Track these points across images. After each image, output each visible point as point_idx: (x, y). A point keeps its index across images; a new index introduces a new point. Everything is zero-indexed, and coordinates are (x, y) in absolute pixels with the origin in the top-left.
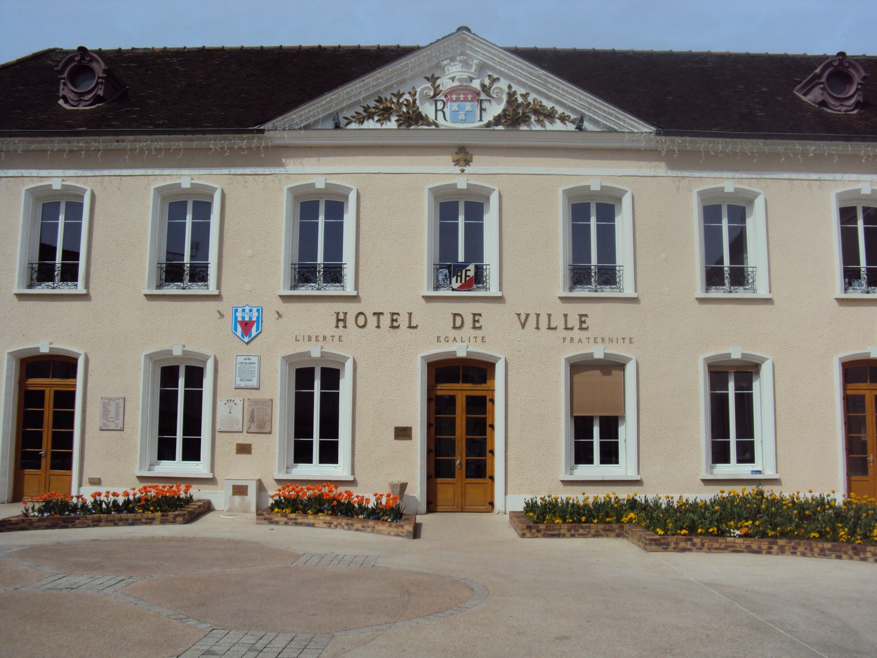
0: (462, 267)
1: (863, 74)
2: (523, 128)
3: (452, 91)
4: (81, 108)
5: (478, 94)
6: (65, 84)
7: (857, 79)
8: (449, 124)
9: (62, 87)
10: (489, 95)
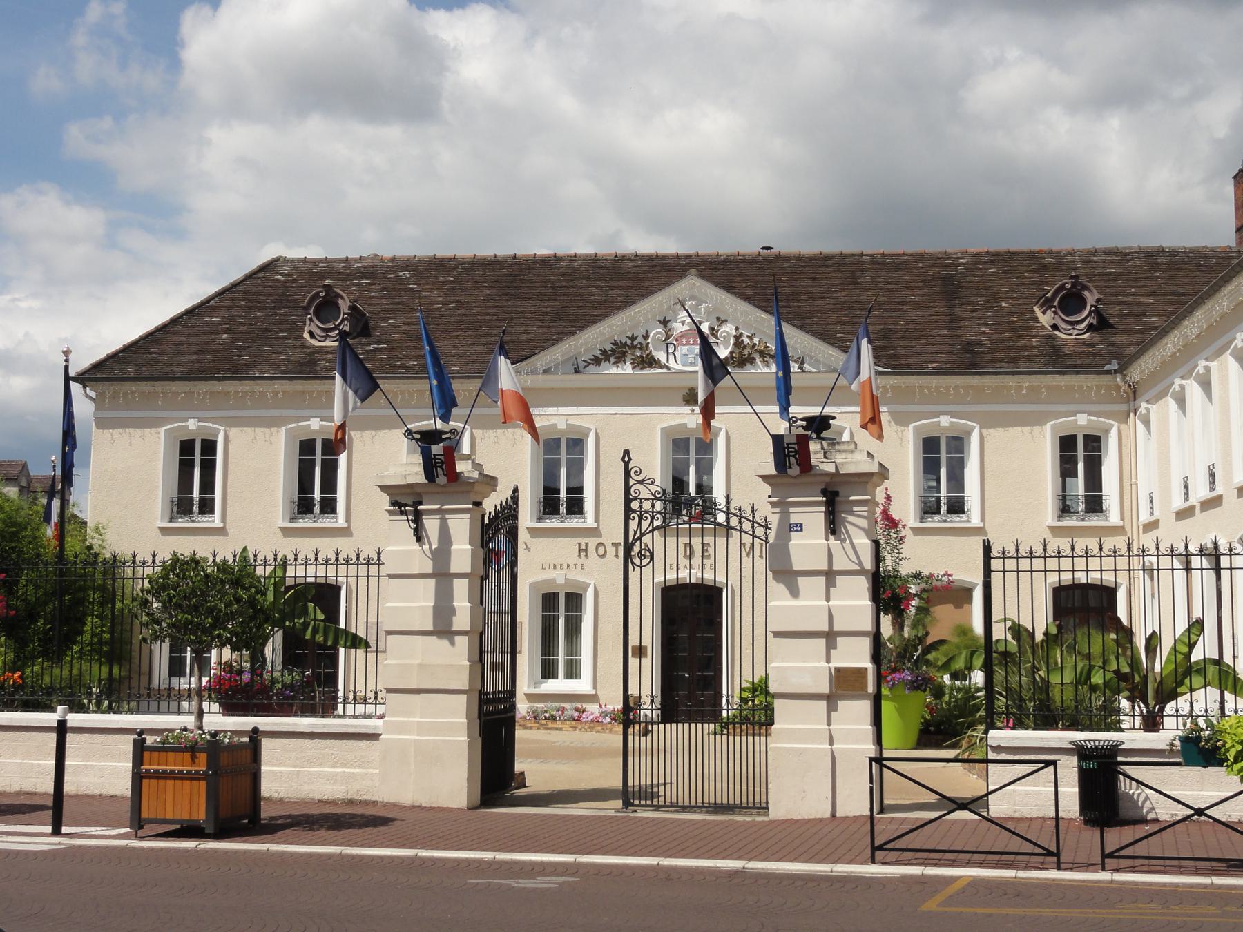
1: (1097, 296)
3: (683, 335)
6: (311, 319)
8: (679, 367)
9: (308, 322)
10: (716, 337)
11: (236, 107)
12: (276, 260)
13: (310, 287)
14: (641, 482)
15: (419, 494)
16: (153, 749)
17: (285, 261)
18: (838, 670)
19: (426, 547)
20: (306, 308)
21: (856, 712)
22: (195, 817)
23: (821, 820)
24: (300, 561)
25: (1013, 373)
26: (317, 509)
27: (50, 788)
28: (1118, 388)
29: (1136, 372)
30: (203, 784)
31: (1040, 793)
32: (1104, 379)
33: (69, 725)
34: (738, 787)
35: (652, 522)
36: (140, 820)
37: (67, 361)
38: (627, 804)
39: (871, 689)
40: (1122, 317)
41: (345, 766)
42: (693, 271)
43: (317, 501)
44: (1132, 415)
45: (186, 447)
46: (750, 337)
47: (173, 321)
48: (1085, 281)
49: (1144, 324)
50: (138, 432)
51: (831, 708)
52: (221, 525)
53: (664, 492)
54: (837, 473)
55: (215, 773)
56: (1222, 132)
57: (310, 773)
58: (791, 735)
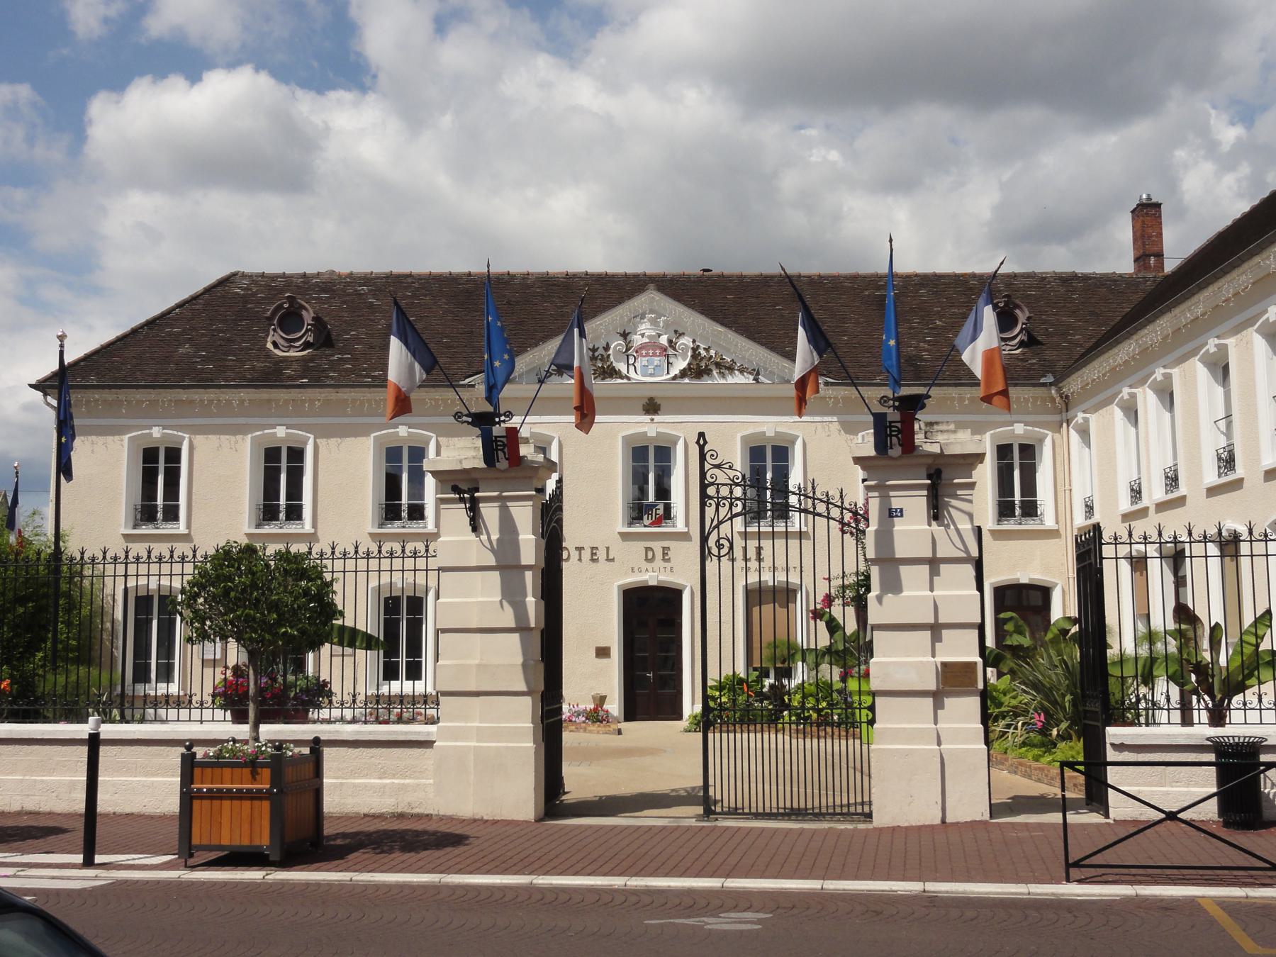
0: (652, 506)
1: (1027, 314)
3: (643, 347)
4: (292, 353)
5: (666, 350)
6: (274, 330)
10: (675, 349)
11: (140, 176)
12: (234, 274)
13: (270, 300)
14: (718, 467)
15: (476, 481)
16: (204, 765)
17: (244, 275)
18: (944, 664)
19: (484, 537)
20: (270, 319)
21: (964, 713)
22: (257, 842)
23: (932, 827)
24: (337, 554)
25: (956, 385)
26: (282, 516)
27: (81, 807)
28: (1053, 400)
29: (1073, 384)
30: (266, 805)
31: (1167, 793)
32: (1040, 392)
33: (102, 737)
35: (730, 508)
36: (190, 847)
37: (62, 346)
38: (708, 813)
40: (1049, 335)
41: (394, 776)
42: (652, 286)
43: (283, 508)
44: (1065, 425)
45: (150, 455)
46: (707, 350)
47: (134, 332)
48: (1017, 301)
50: (101, 440)
51: (938, 705)
52: (186, 532)
53: (744, 476)
54: (942, 455)
55: (281, 791)
56: (987, 214)
57: (355, 785)
58: (896, 735)
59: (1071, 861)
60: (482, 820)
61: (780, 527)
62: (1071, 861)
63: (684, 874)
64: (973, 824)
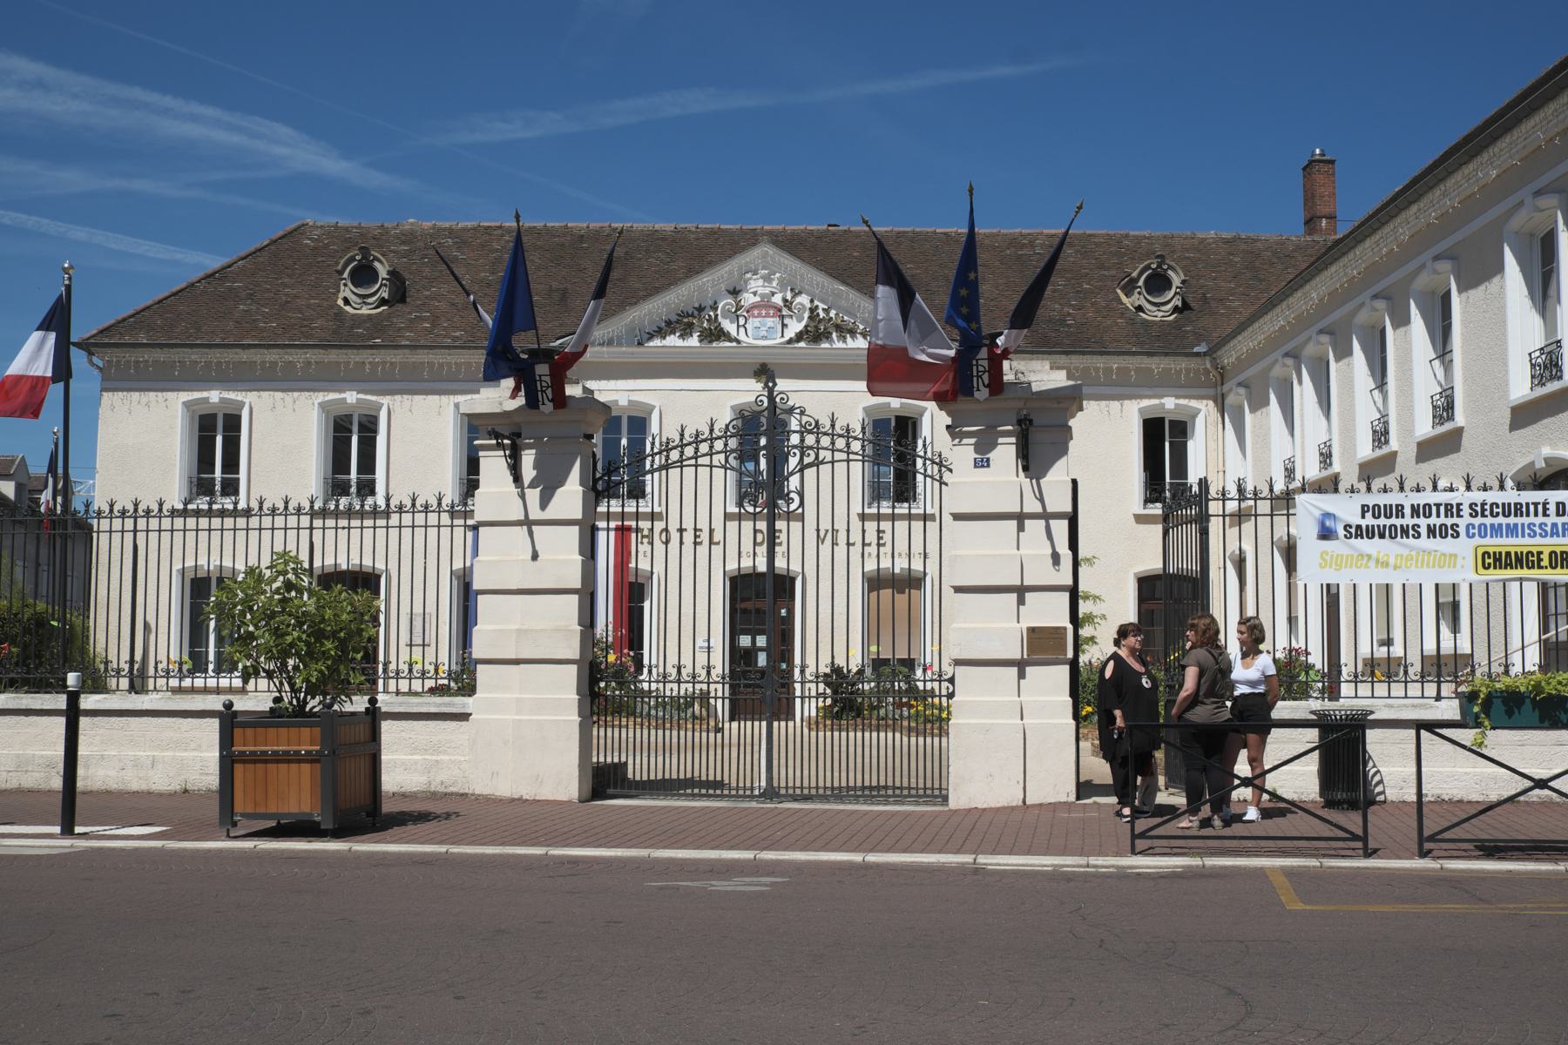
2: (825, 345)
3: (754, 306)
4: (365, 311)
7: (1176, 280)
8: (751, 341)
18: (1032, 630)
23: (1013, 808)
27: (57, 783)
32: (1193, 363)
34: (829, 774)
35: (801, 459)
39: (1070, 654)
49: (1228, 308)
59: (1426, 833)
60: (520, 799)
61: (902, 509)
62: (1426, 833)
63: (804, 849)
64: (1054, 807)
